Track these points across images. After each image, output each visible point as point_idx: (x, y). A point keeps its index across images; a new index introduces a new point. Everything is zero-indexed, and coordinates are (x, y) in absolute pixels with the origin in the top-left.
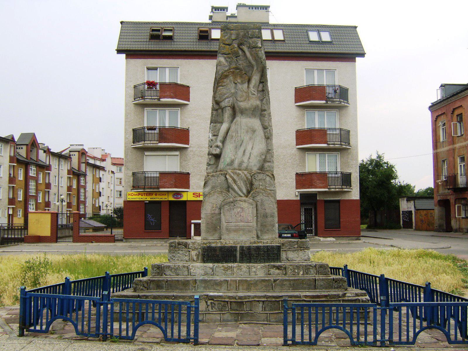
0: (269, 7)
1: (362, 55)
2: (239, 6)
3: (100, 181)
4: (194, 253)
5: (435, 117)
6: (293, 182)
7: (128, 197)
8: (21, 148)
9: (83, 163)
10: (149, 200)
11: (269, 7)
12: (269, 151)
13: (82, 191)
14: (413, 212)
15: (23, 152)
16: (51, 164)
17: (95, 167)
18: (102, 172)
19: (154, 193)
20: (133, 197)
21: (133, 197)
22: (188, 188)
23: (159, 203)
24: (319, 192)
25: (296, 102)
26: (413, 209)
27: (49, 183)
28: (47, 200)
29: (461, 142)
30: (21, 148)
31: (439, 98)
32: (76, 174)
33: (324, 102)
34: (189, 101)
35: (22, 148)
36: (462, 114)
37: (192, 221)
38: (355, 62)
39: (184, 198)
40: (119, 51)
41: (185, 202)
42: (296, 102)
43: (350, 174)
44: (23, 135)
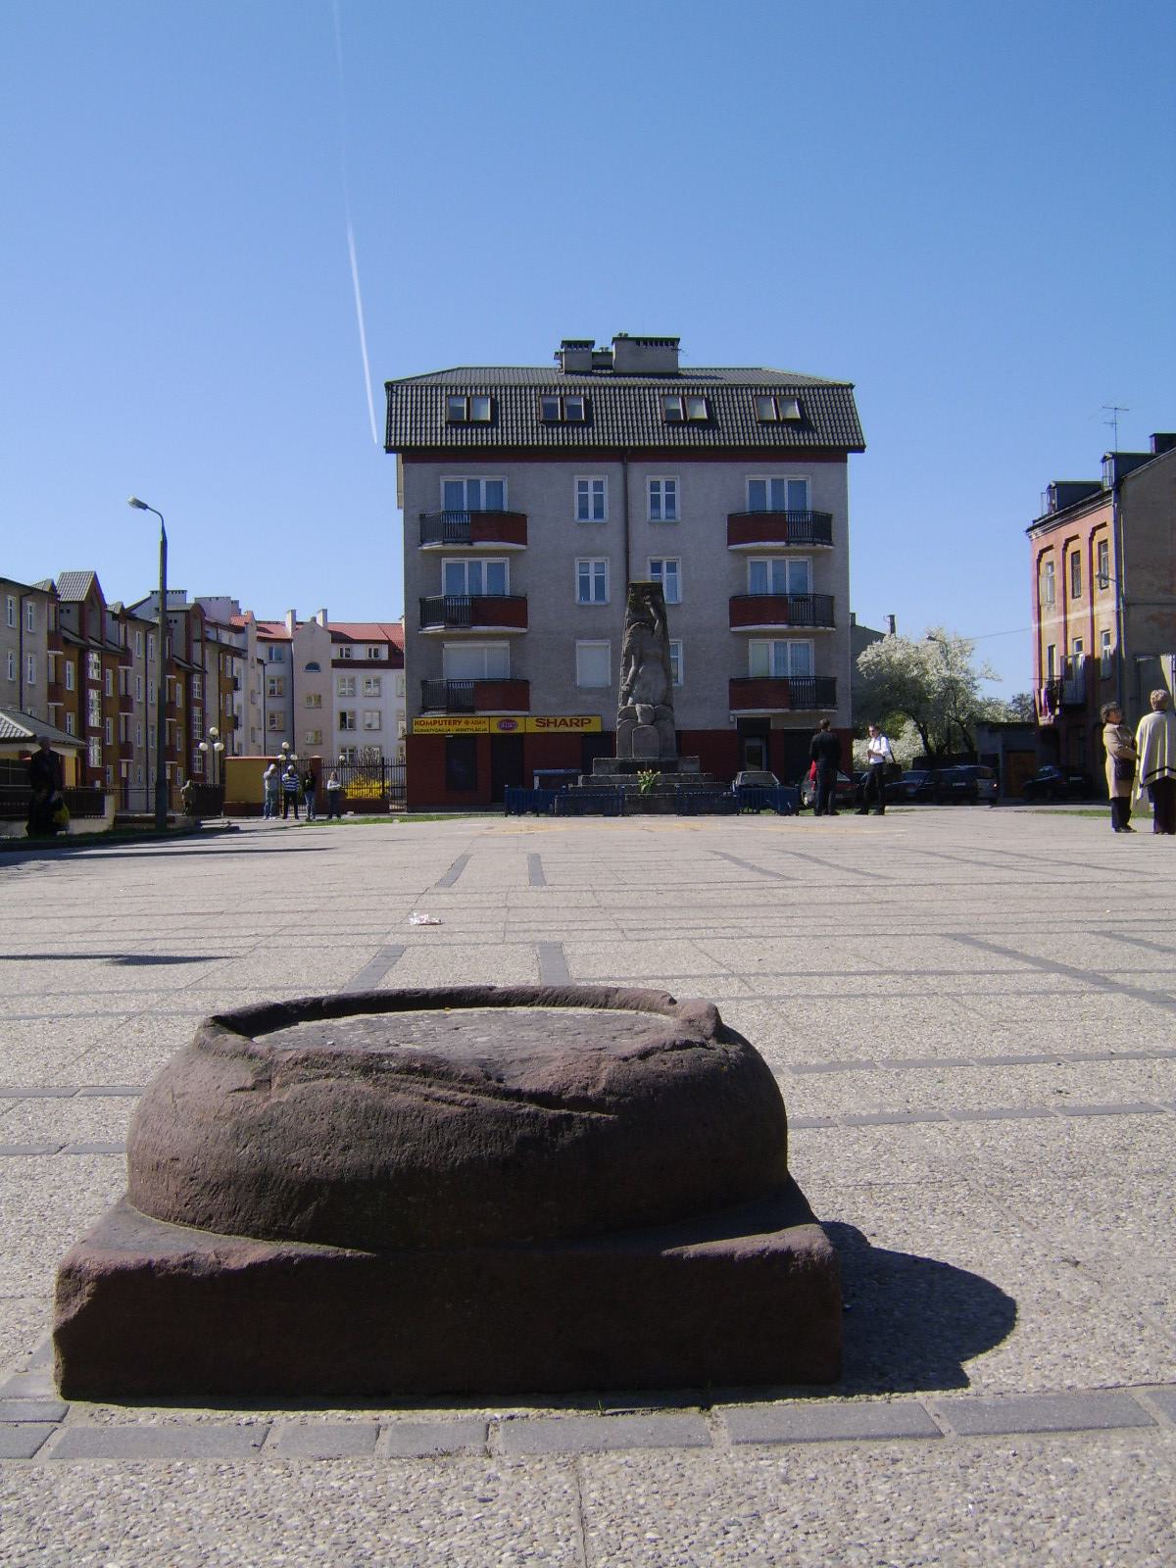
0: (678, 340)
1: (861, 449)
2: (621, 340)
3: (236, 688)
4: (612, 767)
5: (1064, 542)
6: (723, 694)
7: (415, 727)
8: (65, 611)
9: (198, 641)
10: (455, 732)
11: (678, 340)
12: (669, 689)
13: (196, 712)
14: (1001, 758)
15: (71, 622)
16: (129, 645)
17: (227, 650)
18: (238, 662)
19: (464, 720)
20: (425, 727)
21: (425, 727)
22: (527, 709)
23: (473, 737)
24: (774, 714)
25: (731, 541)
26: (1000, 751)
27: (127, 696)
28: (123, 739)
29: (1078, 611)
30: (65, 611)
31: (1046, 513)
32: (180, 667)
33: (783, 543)
34: (524, 542)
35: (68, 611)
36: (1079, 551)
37: (536, 771)
38: (846, 462)
39: (519, 730)
40: (389, 449)
41: (521, 736)
42: (731, 541)
43: (833, 681)
44: (63, 575)
